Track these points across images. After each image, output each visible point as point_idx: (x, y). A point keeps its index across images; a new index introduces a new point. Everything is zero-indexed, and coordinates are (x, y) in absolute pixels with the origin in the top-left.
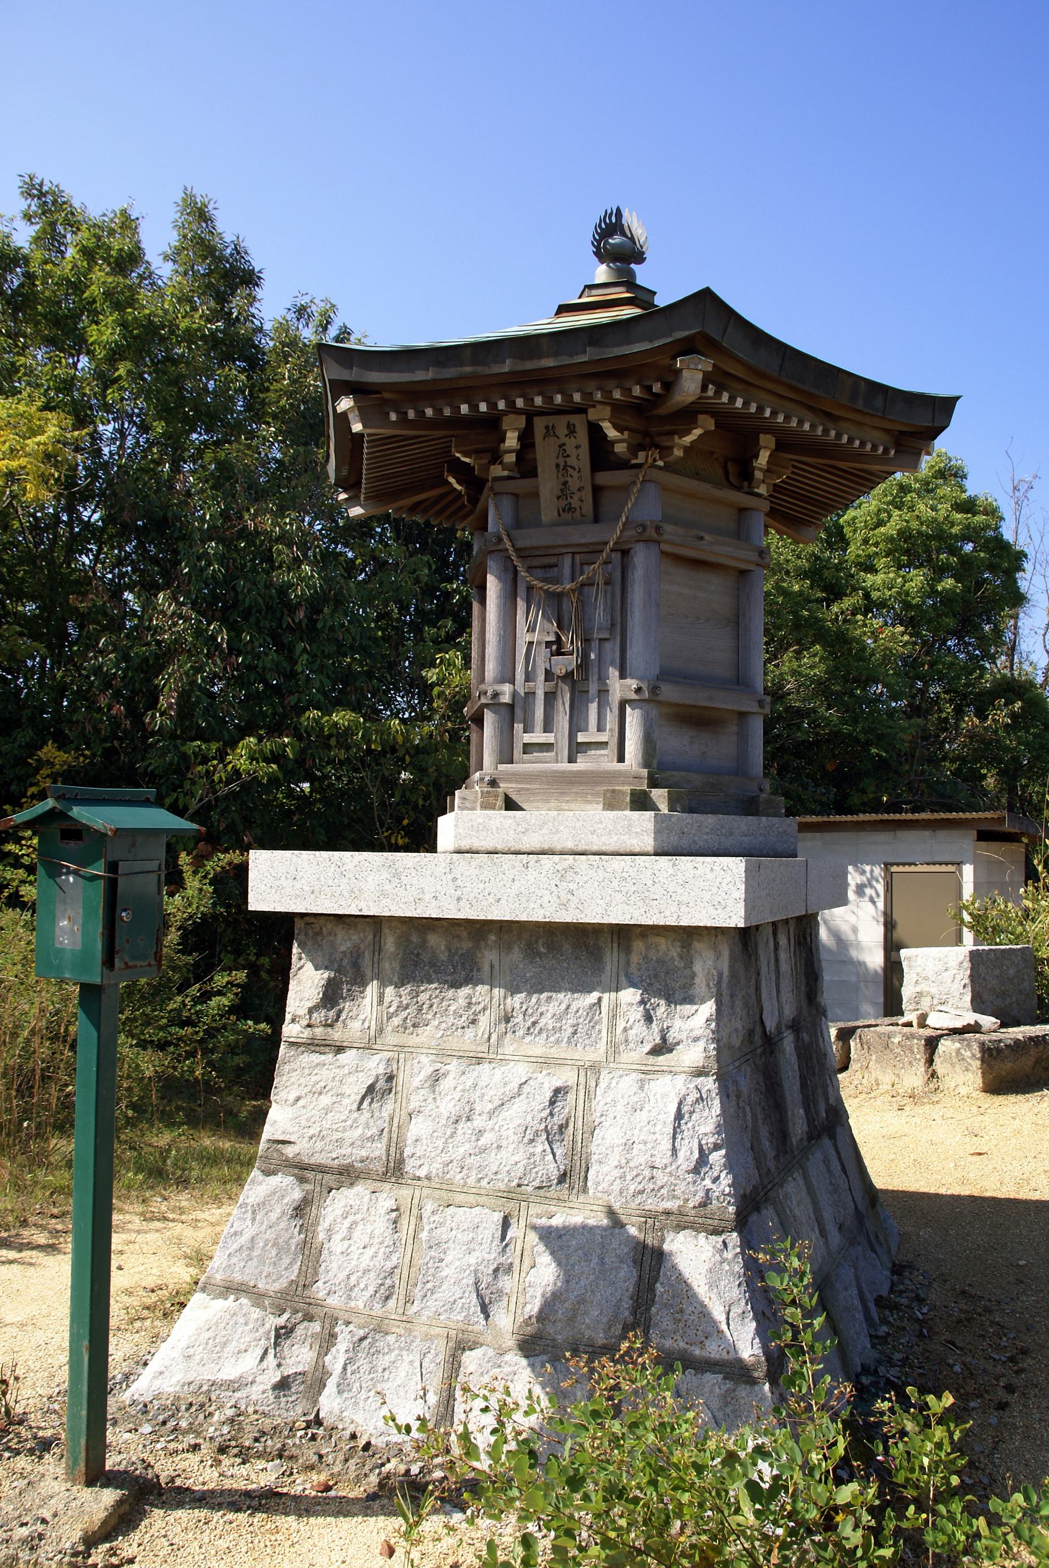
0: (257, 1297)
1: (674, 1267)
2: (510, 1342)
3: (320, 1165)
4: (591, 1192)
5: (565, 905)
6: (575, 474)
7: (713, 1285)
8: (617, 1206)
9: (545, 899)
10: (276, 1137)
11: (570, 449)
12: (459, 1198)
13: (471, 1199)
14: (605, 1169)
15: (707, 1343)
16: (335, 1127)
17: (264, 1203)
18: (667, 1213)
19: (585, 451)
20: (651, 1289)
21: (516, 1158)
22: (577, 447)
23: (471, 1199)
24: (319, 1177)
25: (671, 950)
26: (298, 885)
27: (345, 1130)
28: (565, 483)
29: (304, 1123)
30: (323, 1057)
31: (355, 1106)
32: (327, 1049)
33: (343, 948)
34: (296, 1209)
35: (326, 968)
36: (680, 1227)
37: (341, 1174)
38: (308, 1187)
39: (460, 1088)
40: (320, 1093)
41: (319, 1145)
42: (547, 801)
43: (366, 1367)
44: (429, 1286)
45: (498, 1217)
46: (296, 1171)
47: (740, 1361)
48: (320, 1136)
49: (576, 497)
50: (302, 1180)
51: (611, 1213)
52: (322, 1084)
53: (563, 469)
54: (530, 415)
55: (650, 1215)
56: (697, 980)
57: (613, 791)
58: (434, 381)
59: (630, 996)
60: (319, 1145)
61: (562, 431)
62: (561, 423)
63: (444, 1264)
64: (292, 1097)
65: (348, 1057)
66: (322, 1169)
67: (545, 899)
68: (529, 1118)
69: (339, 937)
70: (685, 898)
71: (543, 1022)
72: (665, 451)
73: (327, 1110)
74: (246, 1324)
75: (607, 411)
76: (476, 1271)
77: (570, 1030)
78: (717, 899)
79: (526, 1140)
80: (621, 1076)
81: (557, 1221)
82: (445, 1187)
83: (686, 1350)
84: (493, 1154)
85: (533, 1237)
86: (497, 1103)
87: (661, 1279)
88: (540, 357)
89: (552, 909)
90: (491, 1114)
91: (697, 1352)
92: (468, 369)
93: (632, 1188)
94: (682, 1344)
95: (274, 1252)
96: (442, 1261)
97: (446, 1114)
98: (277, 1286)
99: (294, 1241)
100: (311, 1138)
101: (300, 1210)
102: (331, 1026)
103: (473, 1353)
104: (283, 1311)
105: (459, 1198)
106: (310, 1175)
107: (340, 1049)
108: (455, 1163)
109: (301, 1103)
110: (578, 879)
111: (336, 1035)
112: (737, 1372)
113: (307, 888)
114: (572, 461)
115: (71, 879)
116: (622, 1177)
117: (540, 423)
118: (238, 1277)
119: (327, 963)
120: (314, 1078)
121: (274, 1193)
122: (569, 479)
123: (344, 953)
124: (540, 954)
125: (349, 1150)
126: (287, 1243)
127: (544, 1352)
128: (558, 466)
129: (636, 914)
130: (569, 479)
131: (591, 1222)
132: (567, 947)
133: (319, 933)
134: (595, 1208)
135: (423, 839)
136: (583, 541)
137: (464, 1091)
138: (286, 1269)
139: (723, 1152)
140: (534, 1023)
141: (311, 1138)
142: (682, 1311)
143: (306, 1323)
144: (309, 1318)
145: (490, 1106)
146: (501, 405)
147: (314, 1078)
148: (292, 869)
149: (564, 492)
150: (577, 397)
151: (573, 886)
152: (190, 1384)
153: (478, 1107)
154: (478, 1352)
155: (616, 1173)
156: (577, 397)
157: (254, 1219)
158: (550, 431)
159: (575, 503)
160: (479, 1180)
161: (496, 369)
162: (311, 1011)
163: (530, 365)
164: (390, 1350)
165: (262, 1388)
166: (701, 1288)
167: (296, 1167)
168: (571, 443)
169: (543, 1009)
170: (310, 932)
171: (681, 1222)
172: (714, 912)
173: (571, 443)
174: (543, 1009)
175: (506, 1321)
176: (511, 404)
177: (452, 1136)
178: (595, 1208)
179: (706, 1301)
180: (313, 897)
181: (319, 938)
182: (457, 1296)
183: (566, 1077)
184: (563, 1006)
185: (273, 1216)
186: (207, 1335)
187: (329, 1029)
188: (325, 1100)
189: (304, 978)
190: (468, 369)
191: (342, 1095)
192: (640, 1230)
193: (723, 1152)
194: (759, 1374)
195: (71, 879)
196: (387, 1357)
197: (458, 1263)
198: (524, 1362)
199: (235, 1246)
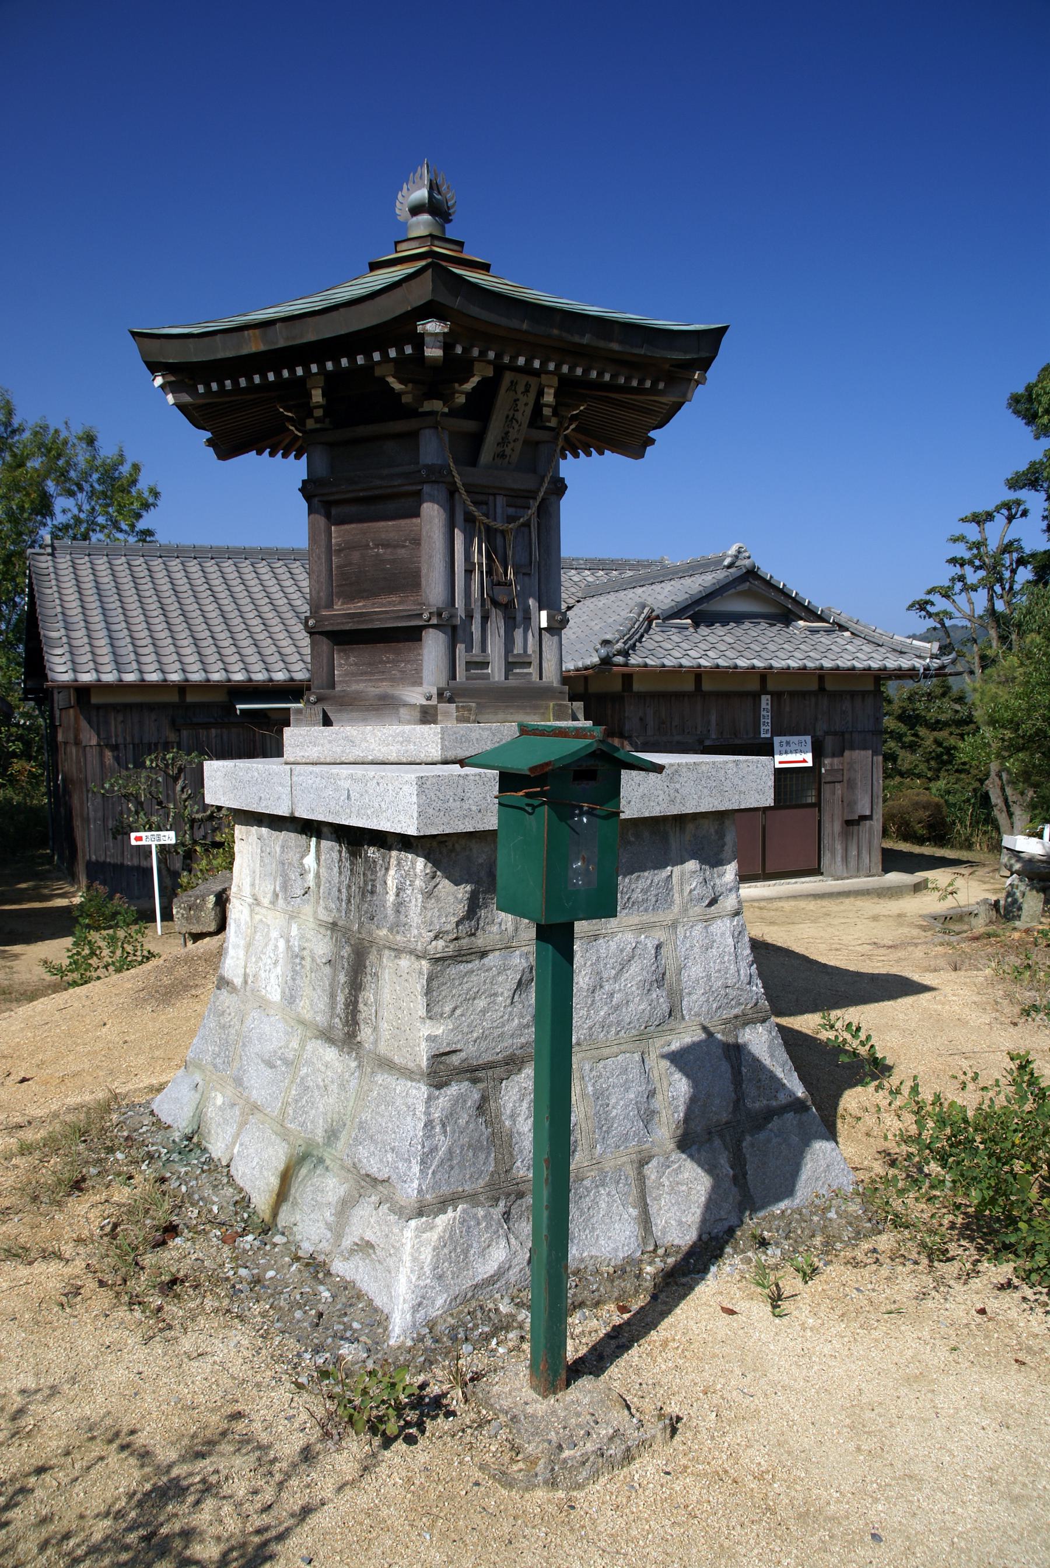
0: (472, 1198)
1: (750, 1053)
2: (671, 1145)
3: (489, 1062)
4: (687, 1018)
5: (673, 801)
6: (516, 427)
7: (772, 1056)
8: (706, 1024)
9: (660, 798)
10: (441, 1051)
11: (521, 406)
12: (606, 1052)
13: (615, 1049)
14: (695, 997)
15: (778, 1095)
16: (495, 1024)
17: (451, 1114)
18: (736, 1017)
19: (529, 410)
20: (740, 1073)
21: (642, 1007)
22: (526, 404)
23: (615, 1049)
24: (490, 1073)
25: (709, 828)
26: (466, 806)
27: (503, 1025)
28: (507, 433)
29: (465, 1030)
30: (470, 966)
31: (509, 1001)
32: (473, 957)
33: (480, 861)
34: (478, 1108)
35: (467, 882)
36: (745, 1024)
37: (507, 1064)
38: (481, 1086)
39: (589, 963)
40: (474, 999)
41: (484, 1045)
42: (496, 714)
43: (578, 1213)
44: (604, 1128)
45: (637, 1057)
46: (468, 1075)
47: (798, 1099)
48: (483, 1037)
49: (510, 446)
50: (475, 1081)
51: (705, 1029)
52: (475, 990)
53: (510, 420)
54: (500, 369)
55: (726, 1022)
56: (726, 848)
57: (560, 705)
58: (526, 332)
59: (692, 865)
60: (484, 1045)
61: (521, 388)
62: (523, 380)
63: (610, 1107)
64: (447, 1009)
65: (491, 960)
66: (491, 1066)
67: (660, 798)
68: (644, 973)
69: (474, 851)
70: (743, 789)
71: (635, 896)
72: (446, 399)
73: (484, 1012)
74: (479, 1224)
75: (555, 381)
76: (637, 1102)
77: (654, 899)
78: (760, 787)
79: (645, 991)
80: (692, 927)
81: (675, 1046)
82: (593, 1046)
83: (768, 1106)
84: (624, 1010)
85: (665, 1064)
86: (618, 967)
87: (744, 1063)
88: (611, 340)
89: (665, 806)
90: (616, 978)
91: (774, 1104)
92: (556, 332)
93: (714, 1006)
94: (765, 1102)
95: (471, 1154)
96: (608, 1105)
97: (585, 987)
98: (482, 1182)
99: (484, 1137)
100: (475, 1041)
101: (481, 1108)
102: (473, 935)
103: (650, 1165)
104: (497, 1200)
105: (606, 1052)
106: (481, 1074)
107: (483, 954)
108: (597, 1026)
109: (458, 1012)
110: (681, 780)
111: (480, 941)
112: (798, 1106)
113: (474, 808)
114: (519, 416)
115: (585, 820)
116: (707, 1001)
117: (508, 377)
118: (445, 1190)
119: (466, 877)
120: (465, 987)
121: (457, 1101)
122: (511, 430)
123: (481, 864)
124: (629, 842)
125: (510, 1041)
126: (479, 1141)
127: (694, 1143)
128: (507, 417)
129: (716, 803)
130: (511, 430)
131: (696, 1039)
132: (646, 834)
133: (453, 850)
134: (694, 1028)
135: (273, 749)
136: (515, 486)
137: (591, 965)
138: (484, 1163)
139: (755, 966)
140: (629, 898)
141: (475, 1041)
142: (760, 1080)
143: (519, 1202)
144: (521, 1195)
145: (613, 972)
146: (475, 352)
147: (465, 987)
148: (460, 790)
149: (504, 441)
150: (537, 364)
151: (678, 786)
152: (455, 1298)
153: (605, 975)
154: (654, 1163)
155: (703, 998)
156: (537, 364)
157: (445, 1132)
158: (513, 384)
159: (508, 451)
160: (617, 1033)
161: (576, 339)
162: (458, 924)
163: (602, 344)
164: (589, 1192)
165: (518, 1269)
166: (767, 1061)
167: (467, 1071)
168: (523, 399)
169: (633, 886)
170: (445, 851)
171: (745, 1020)
172: (758, 797)
173: (523, 399)
174: (633, 886)
175: (665, 1132)
176: (483, 353)
177: (592, 1005)
178: (694, 1028)
179: (772, 1068)
180: (480, 815)
181: (453, 855)
182: (628, 1127)
183: (660, 935)
184: (649, 881)
185: (462, 1122)
186: (446, 1251)
187: (473, 938)
188: (481, 1003)
189: (443, 895)
190: (556, 332)
191: (495, 995)
192: (723, 1034)
193: (755, 966)
194: (809, 1103)
195: (585, 820)
196: (587, 1199)
197: (622, 1103)
198: (684, 1156)
199: (435, 1163)
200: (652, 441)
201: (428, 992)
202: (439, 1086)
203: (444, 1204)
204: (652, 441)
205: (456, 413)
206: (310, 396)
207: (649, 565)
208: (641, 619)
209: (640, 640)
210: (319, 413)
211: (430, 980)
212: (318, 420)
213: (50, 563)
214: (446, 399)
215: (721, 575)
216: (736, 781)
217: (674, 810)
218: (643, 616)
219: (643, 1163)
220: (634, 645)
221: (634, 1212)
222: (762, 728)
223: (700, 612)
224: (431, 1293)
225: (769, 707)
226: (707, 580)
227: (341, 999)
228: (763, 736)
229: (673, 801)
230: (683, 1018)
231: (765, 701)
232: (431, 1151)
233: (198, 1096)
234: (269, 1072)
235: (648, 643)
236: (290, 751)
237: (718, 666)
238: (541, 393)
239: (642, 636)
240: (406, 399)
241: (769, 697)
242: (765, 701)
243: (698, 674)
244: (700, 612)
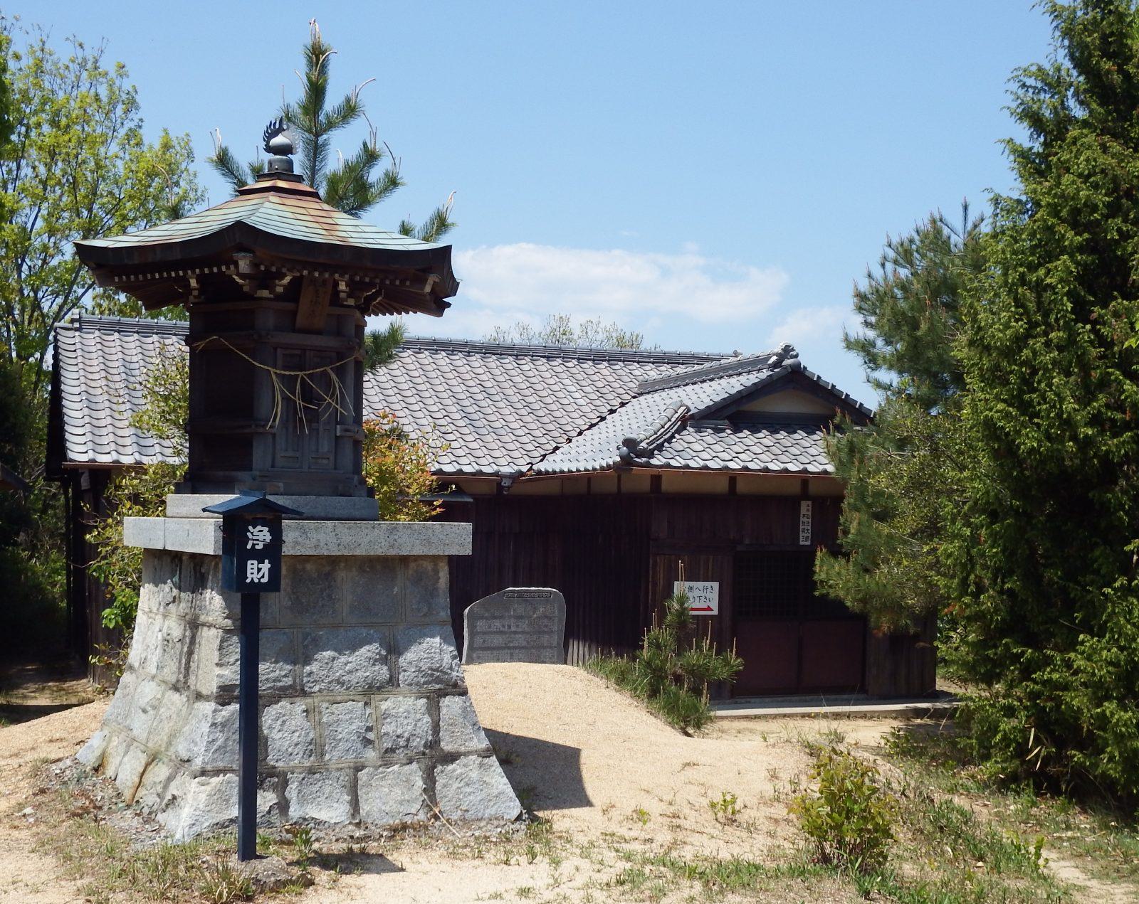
12: (339, 698)
14: (407, 674)
25: (429, 566)
118: (221, 765)
200: (449, 305)
201: (221, 648)
202: (223, 704)
203: (217, 772)
204: (449, 305)
205: (278, 298)
206: (189, 285)
207: (719, 360)
208: (673, 420)
209: (669, 441)
210: (195, 293)
211: (222, 641)
212: (195, 297)
213: (77, 340)
214: (271, 288)
215: (764, 374)
216: (441, 537)
217: (393, 552)
218: (676, 416)
219: (358, 768)
220: (662, 445)
221: (348, 798)
222: (801, 535)
223: (734, 415)
224: (201, 819)
225: (810, 513)
226: (734, 385)
227: (184, 661)
228: (801, 543)
229: (392, 546)
230: (399, 685)
231: (805, 508)
232: (213, 740)
233: (105, 743)
234: (143, 716)
235: (678, 444)
236: (170, 510)
237: (767, 470)
238: (336, 284)
239: (673, 437)
240: (246, 289)
241: (810, 503)
242: (805, 508)
243: (732, 477)
244: (734, 415)
